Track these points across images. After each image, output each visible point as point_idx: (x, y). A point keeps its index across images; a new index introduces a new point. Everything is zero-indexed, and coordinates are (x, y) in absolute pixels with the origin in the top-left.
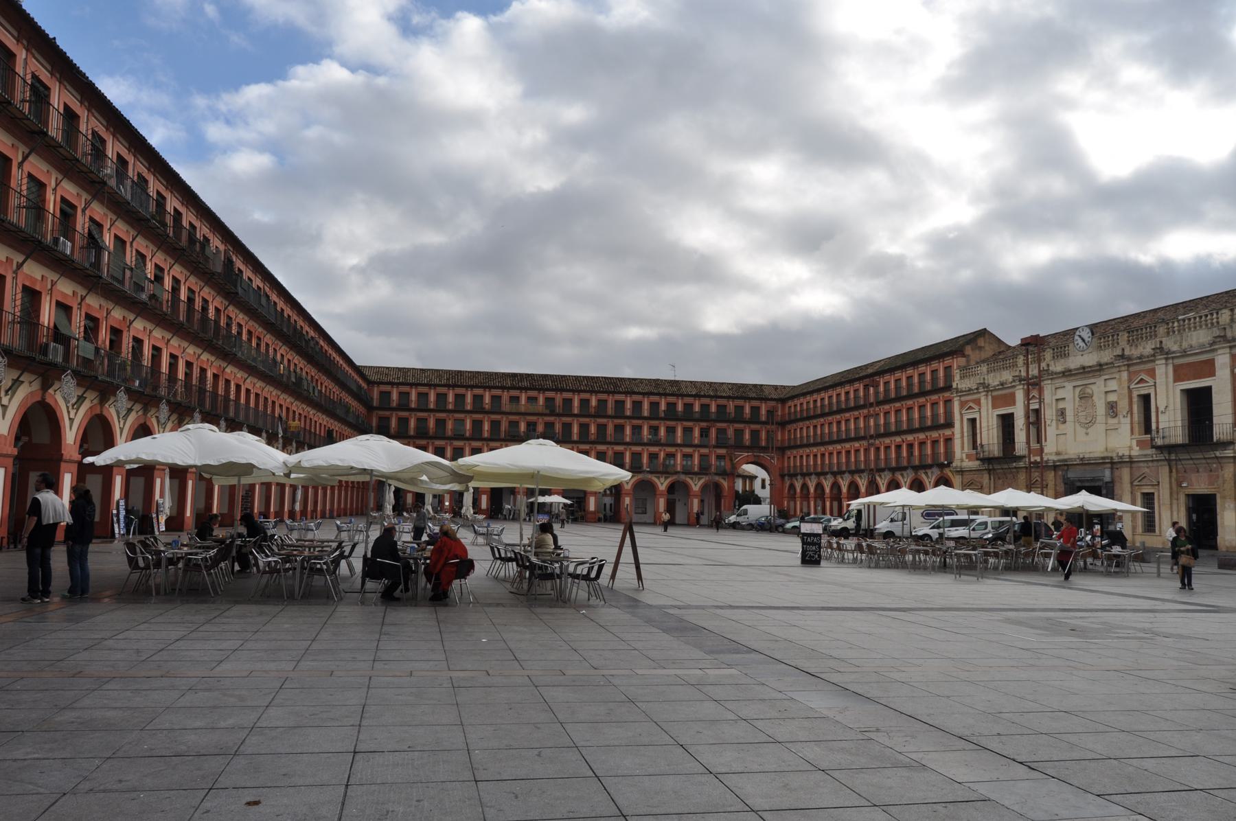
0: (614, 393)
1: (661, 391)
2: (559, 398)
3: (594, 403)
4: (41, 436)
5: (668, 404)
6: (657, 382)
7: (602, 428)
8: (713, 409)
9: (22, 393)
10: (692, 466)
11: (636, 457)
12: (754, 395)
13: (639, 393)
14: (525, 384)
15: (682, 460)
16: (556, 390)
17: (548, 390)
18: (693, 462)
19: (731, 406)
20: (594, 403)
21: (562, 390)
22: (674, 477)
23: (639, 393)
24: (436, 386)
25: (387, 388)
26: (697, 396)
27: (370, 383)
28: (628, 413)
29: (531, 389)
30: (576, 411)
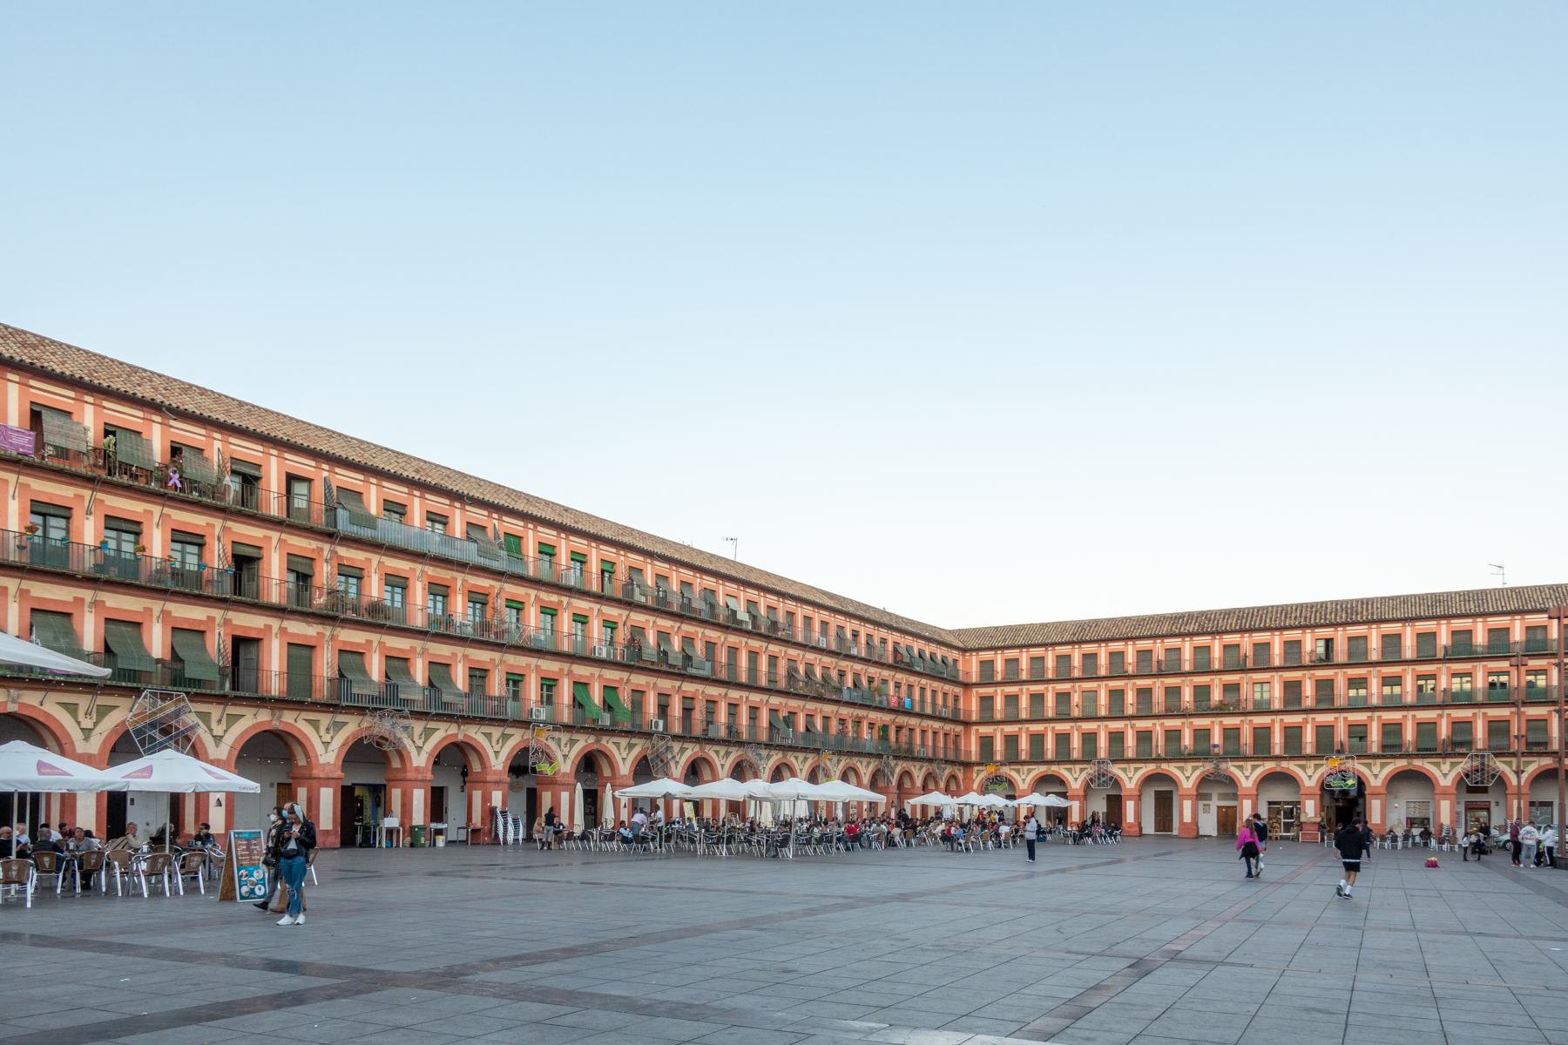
1: (1439, 611)
9: (842, 764)
14: (1191, 628)
19: (1277, 642)
22: (1209, 767)
29: (1198, 634)
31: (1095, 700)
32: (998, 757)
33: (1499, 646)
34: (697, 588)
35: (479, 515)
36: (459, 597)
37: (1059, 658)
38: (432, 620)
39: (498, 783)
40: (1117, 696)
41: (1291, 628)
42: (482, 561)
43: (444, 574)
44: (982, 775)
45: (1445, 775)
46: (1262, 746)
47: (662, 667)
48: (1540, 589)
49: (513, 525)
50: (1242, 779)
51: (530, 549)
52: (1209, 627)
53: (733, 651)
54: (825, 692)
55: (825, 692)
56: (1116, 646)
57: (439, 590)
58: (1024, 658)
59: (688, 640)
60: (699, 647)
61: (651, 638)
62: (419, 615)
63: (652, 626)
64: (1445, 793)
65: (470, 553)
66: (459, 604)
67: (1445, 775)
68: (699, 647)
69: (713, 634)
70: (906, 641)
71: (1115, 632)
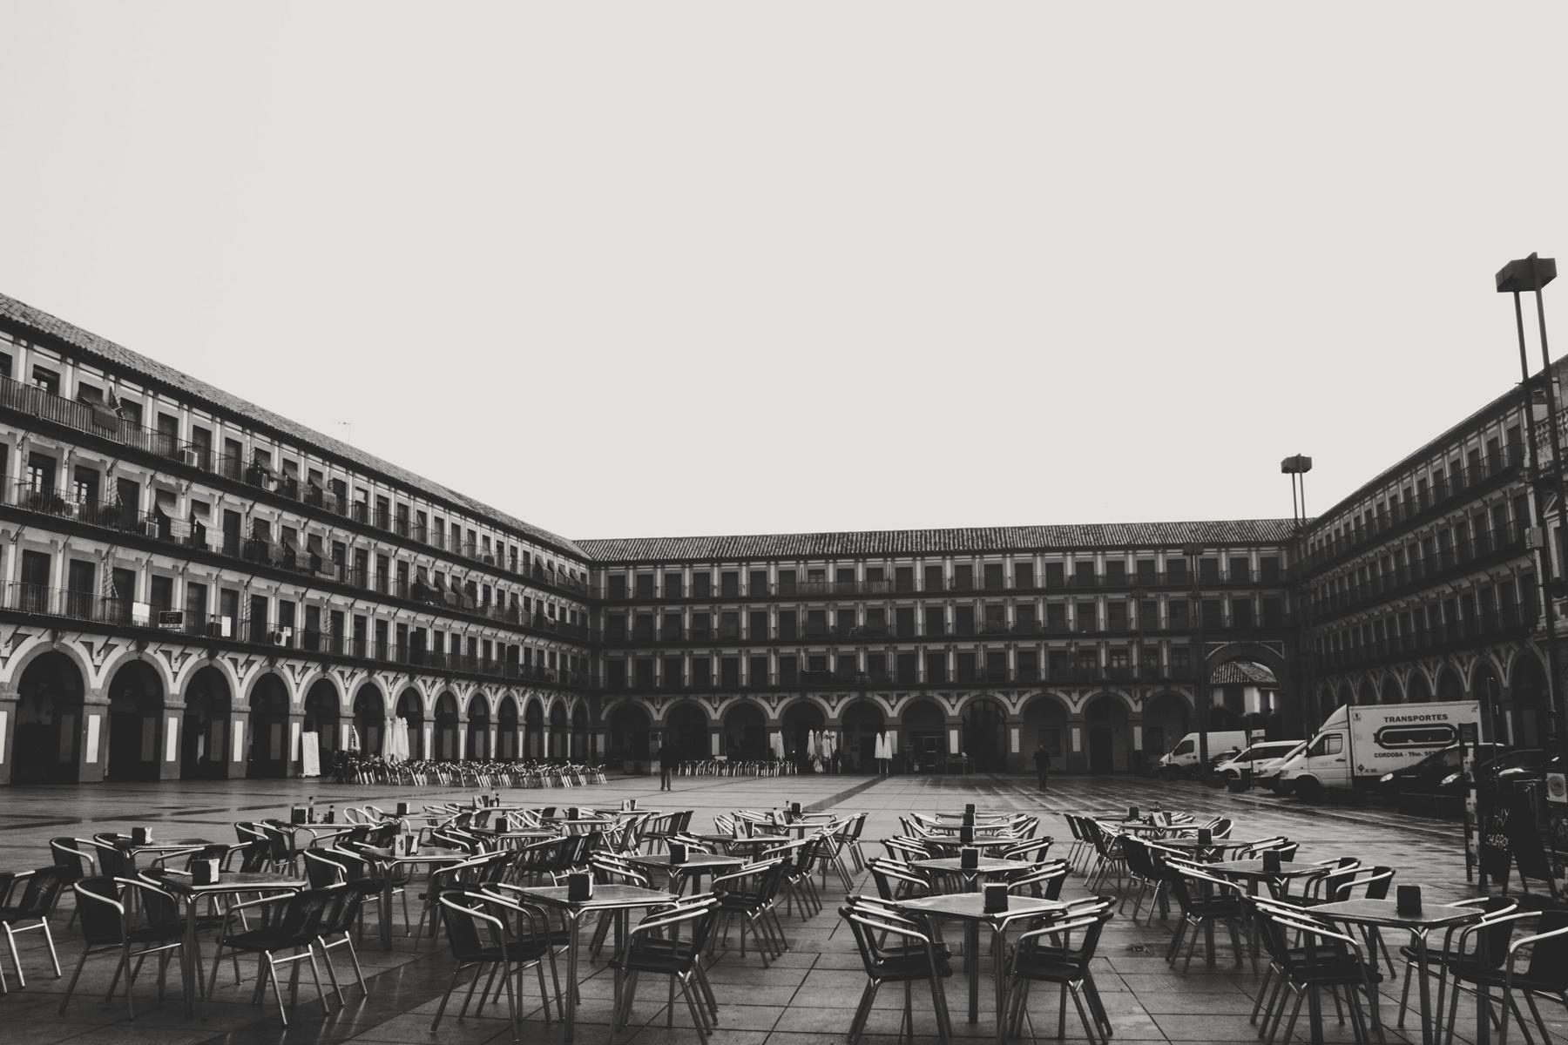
0: (982, 552)
1: (1064, 543)
2: (889, 567)
3: (949, 572)
4: (449, 710)
5: (958, 568)
6: (1061, 531)
7: (964, 614)
8: (773, 578)
10: (1129, 668)
11: (1484, 673)
12: (1236, 538)
13: (1026, 550)
14: (834, 549)
15: (1140, 658)
16: (885, 555)
17: (870, 555)
18: (1129, 660)
19: (978, 566)
20: (949, 572)
21: (895, 555)
23: (1026, 550)
24: (691, 562)
25: (647, 569)
26: (1130, 547)
27: (593, 565)
28: (1040, 584)
29: (841, 556)
30: (1040, 584)
31: (738, 622)
32: (920, 632)
33: (817, 632)
34: (326, 479)
35: (93, 377)
36: (65, 472)
37: (988, 567)
38: (33, 500)
39: (97, 705)
40: (759, 620)
41: (932, 553)
42: (99, 432)
43: (48, 444)
44: (609, 708)
45: (1075, 703)
46: (906, 678)
47: (286, 569)
48: (1146, 526)
49: (129, 391)
50: (711, 711)
51: (149, 421)
52: (852, 549)
53: (362, 555)
54: (459, 606)
55: (459, 606)
56: (758, 566)
57: (43, 463)
58: (978, 566)
59: (315, 540)
60: (326, 546)
61: (275, 534)
62: (15, 490)
63: (278, 520)
64: (1076, 721)
65: (79, 422)
66: (64, 482)
67: (1075, 703)
68: (326, 546)
69: (341, 534)
70: (536, 551)
71: (755, 551)
